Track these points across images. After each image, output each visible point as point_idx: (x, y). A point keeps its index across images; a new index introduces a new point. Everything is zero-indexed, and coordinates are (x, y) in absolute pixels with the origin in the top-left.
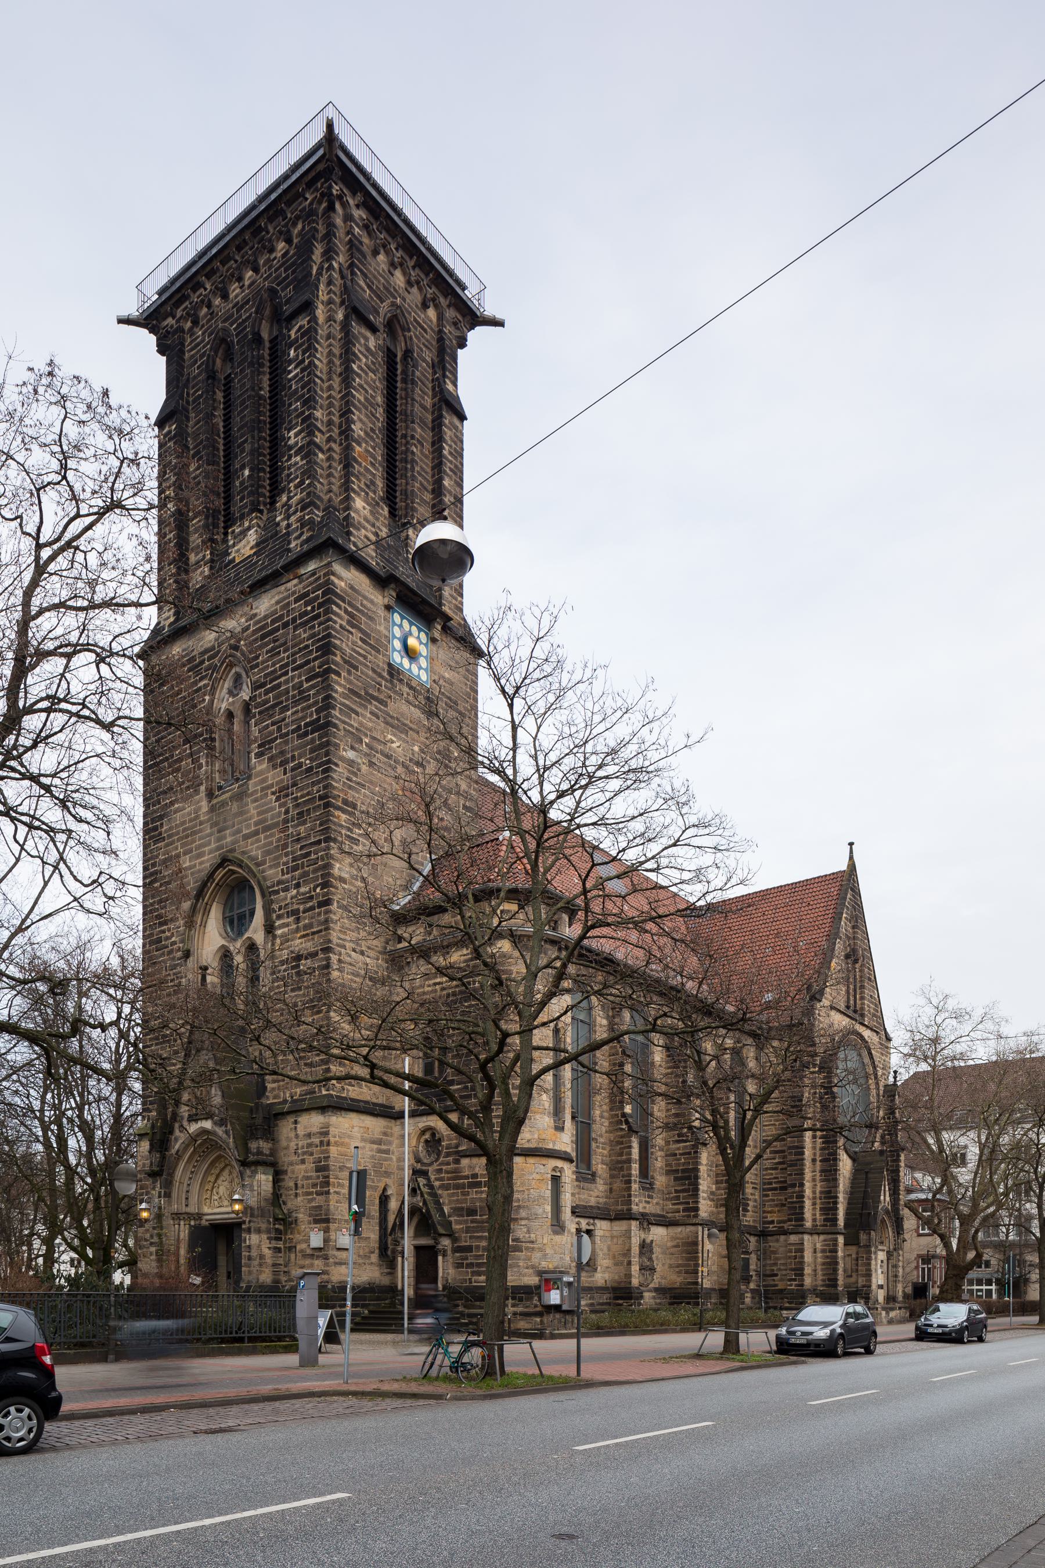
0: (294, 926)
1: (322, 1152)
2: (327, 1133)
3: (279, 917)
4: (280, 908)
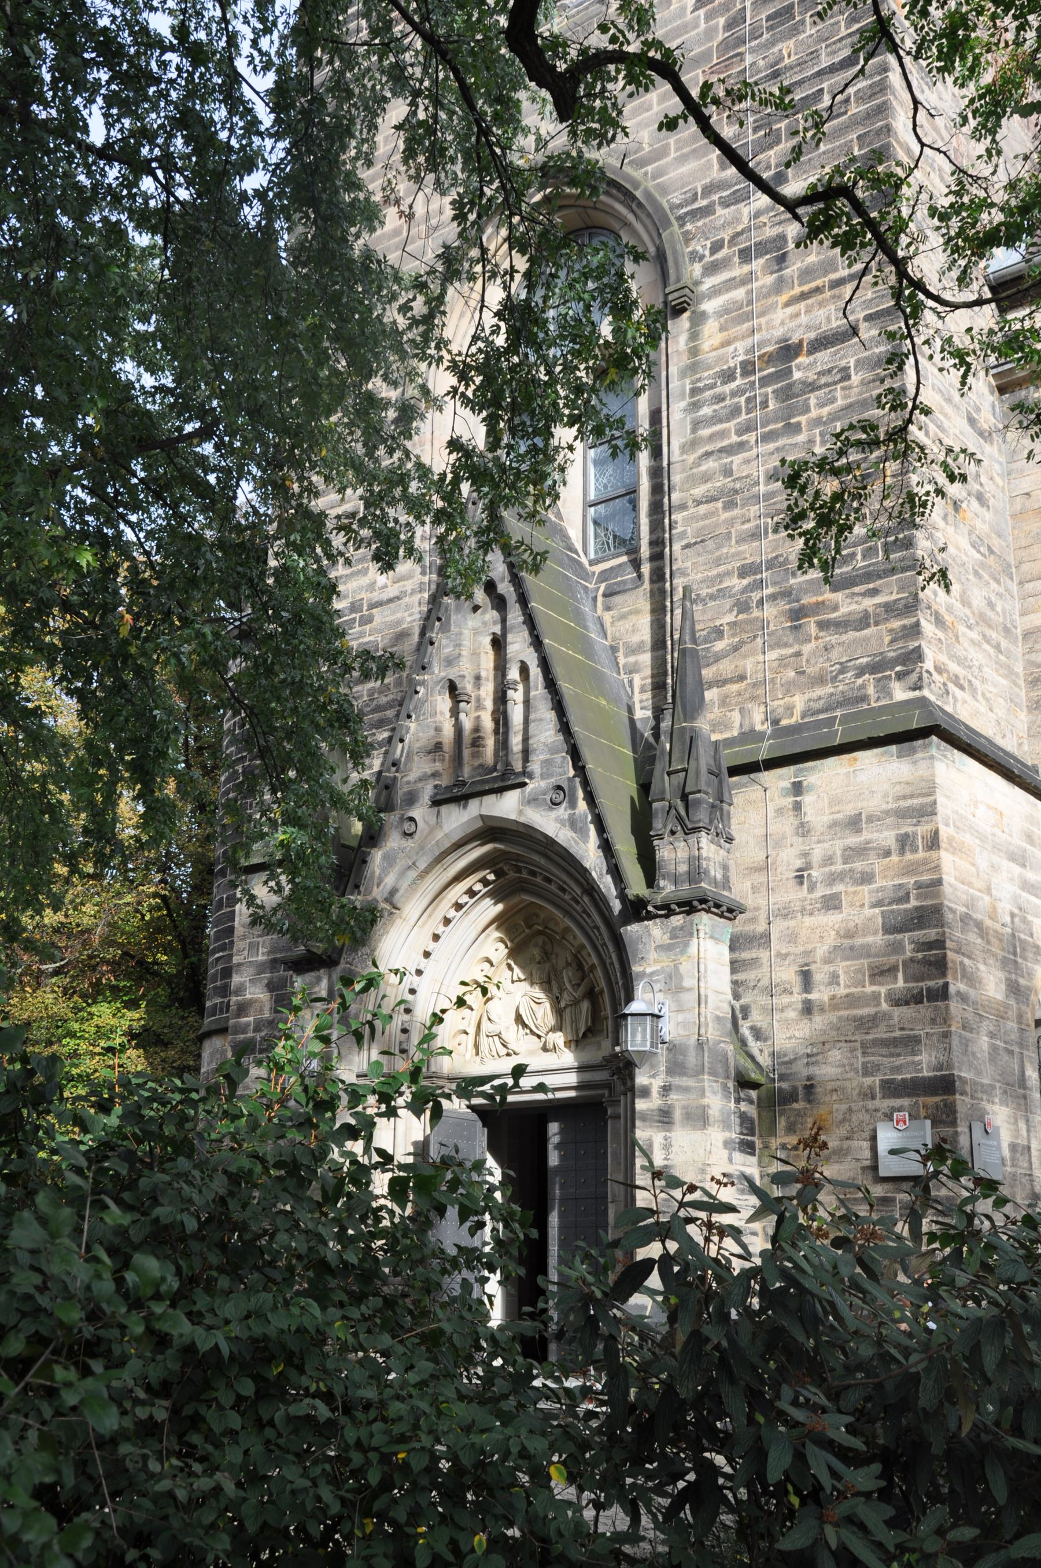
0: (770, 279)
1: (909, 870)
2: (929, 811)
3: (712, 269)
4: (716, 247)
